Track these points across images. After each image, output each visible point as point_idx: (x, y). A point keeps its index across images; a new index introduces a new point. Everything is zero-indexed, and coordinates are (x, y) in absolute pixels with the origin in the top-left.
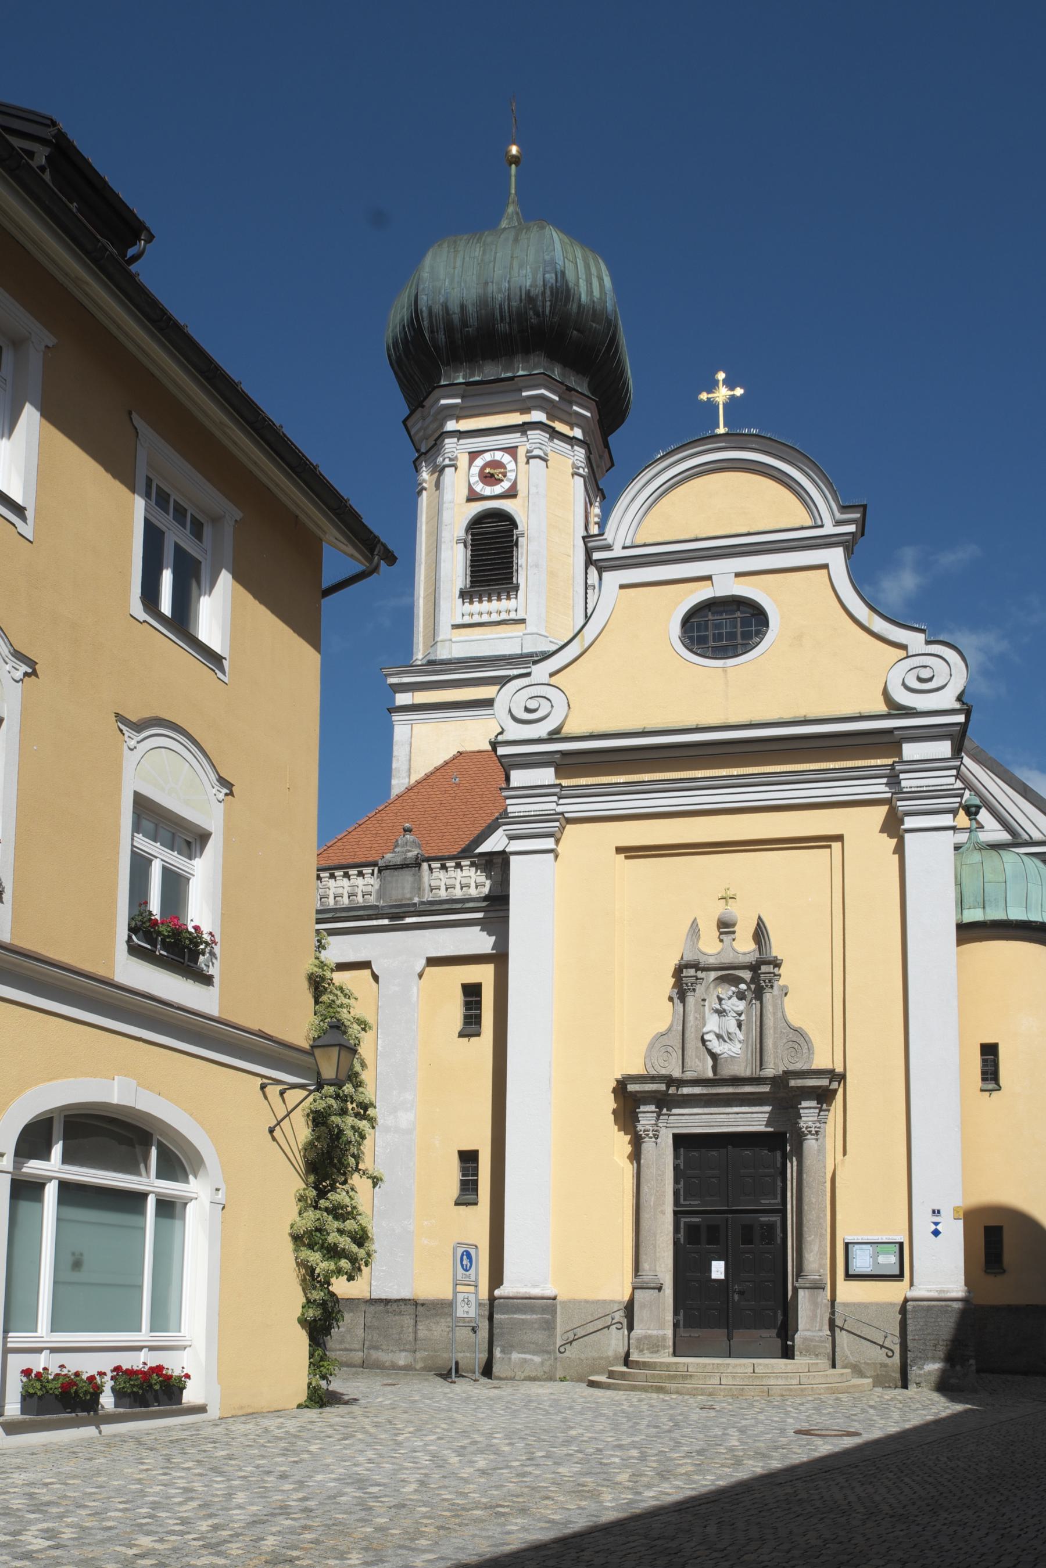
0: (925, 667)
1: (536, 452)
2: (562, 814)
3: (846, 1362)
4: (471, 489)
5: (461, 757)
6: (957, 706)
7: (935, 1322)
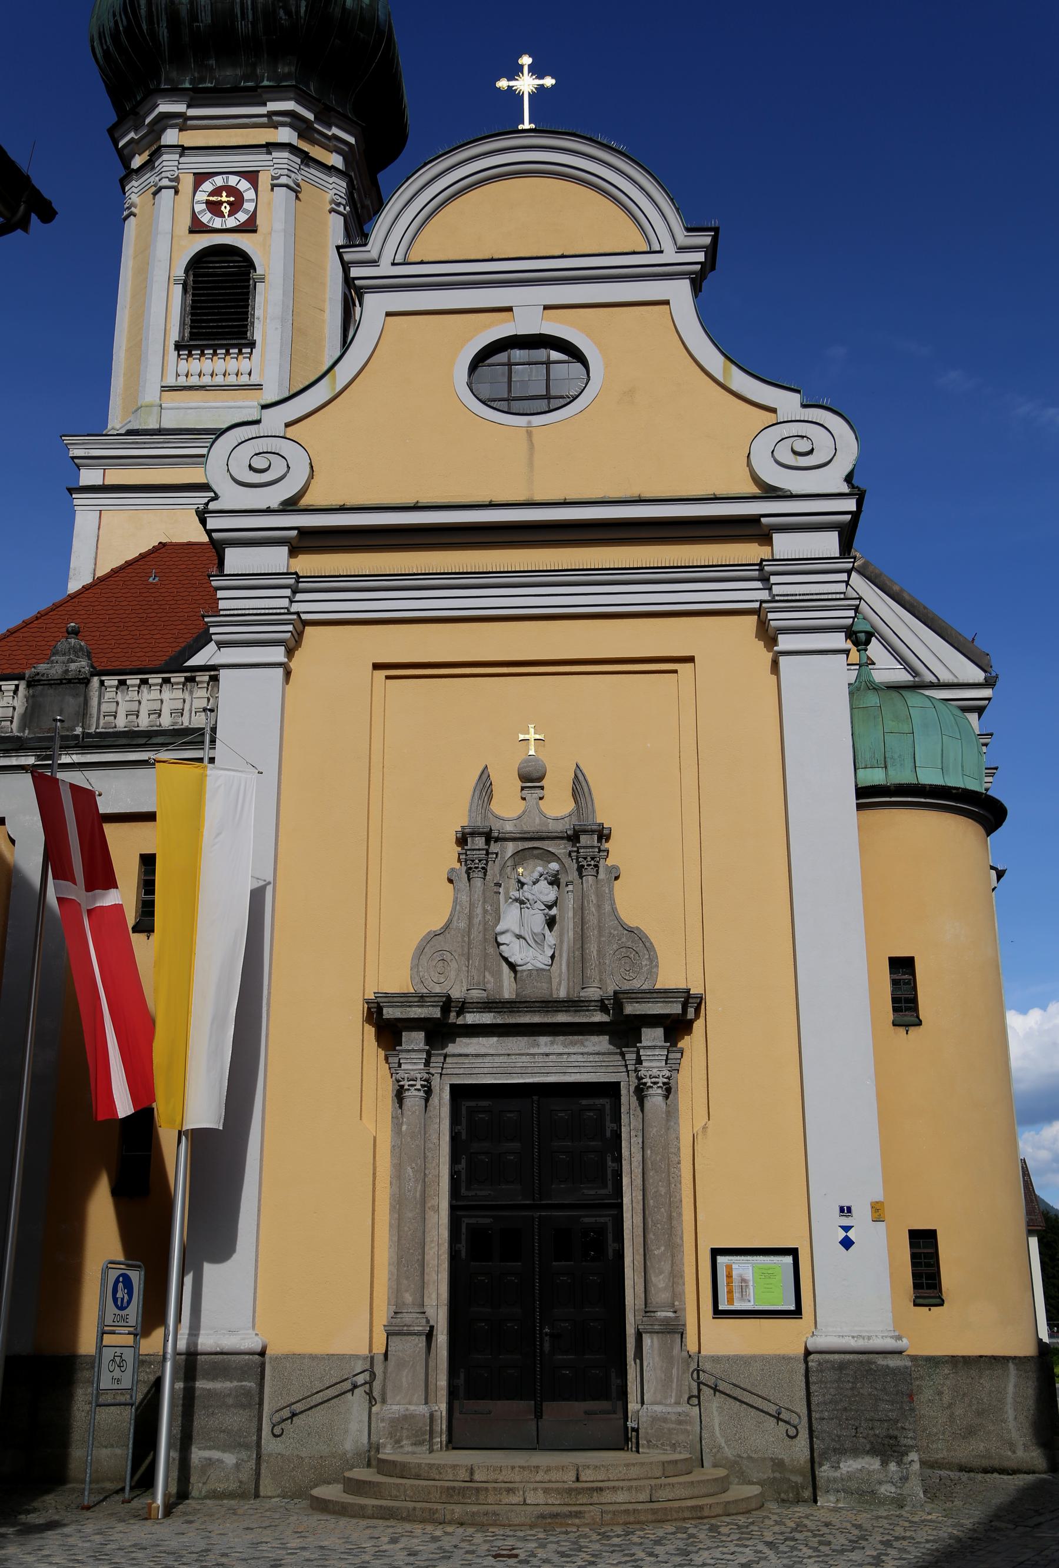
0: (803, 437)
1: (283, 180)
2: (298, 613)
3: (719, 1456)
4: (194, 217)
5: (163, 550)
6: (845, 489)
7: (852, 1389)
